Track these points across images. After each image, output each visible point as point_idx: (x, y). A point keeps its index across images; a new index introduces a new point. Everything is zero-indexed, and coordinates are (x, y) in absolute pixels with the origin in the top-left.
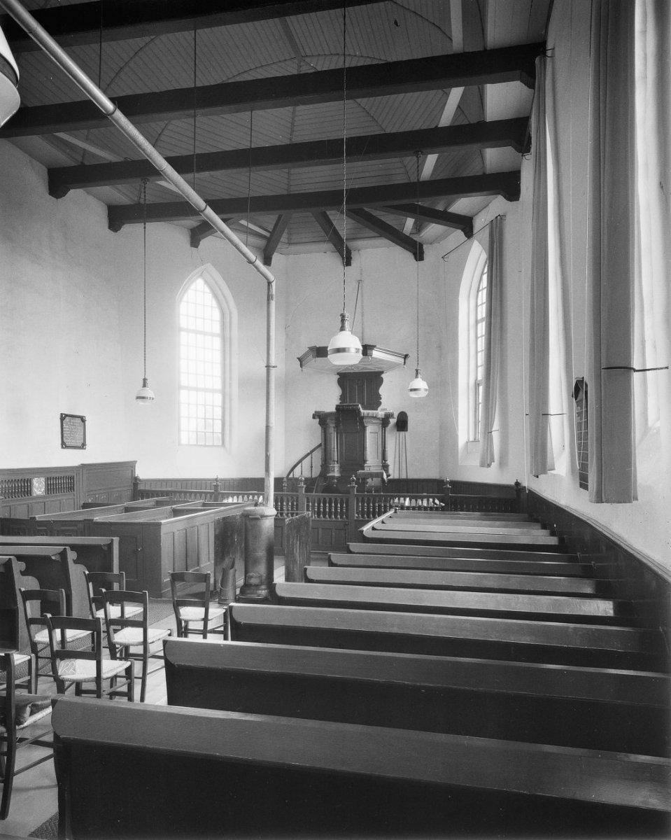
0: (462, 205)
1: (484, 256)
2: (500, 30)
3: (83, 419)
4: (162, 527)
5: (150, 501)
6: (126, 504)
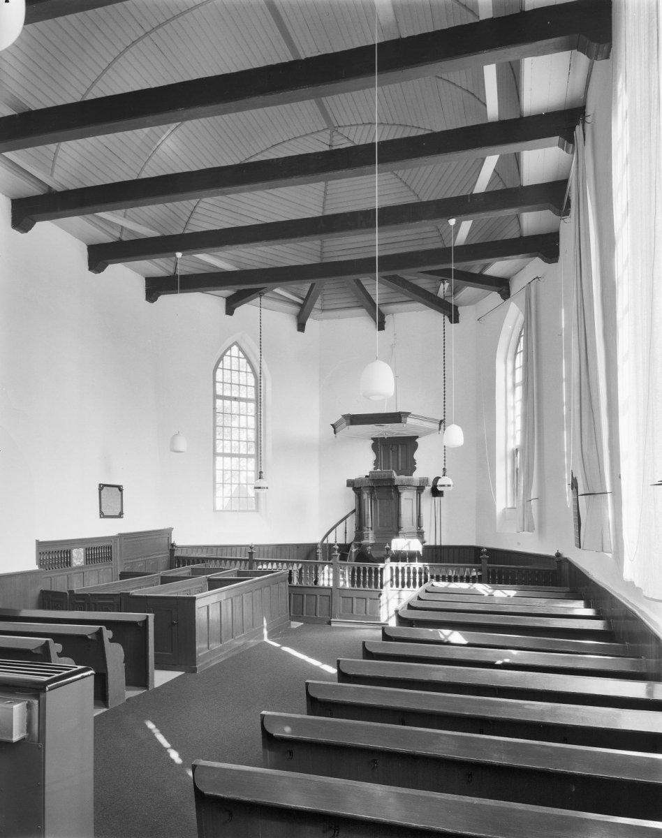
0: (498, 268)
1: (521, 318)
3: (120, 488)
4: (197, 602)
5: (184, 570)
6: (162, 573)
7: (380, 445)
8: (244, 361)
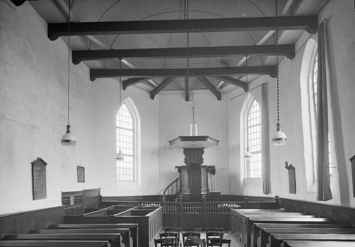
2: (303, 9)
7: (187, 151)
8: (128, 112)
